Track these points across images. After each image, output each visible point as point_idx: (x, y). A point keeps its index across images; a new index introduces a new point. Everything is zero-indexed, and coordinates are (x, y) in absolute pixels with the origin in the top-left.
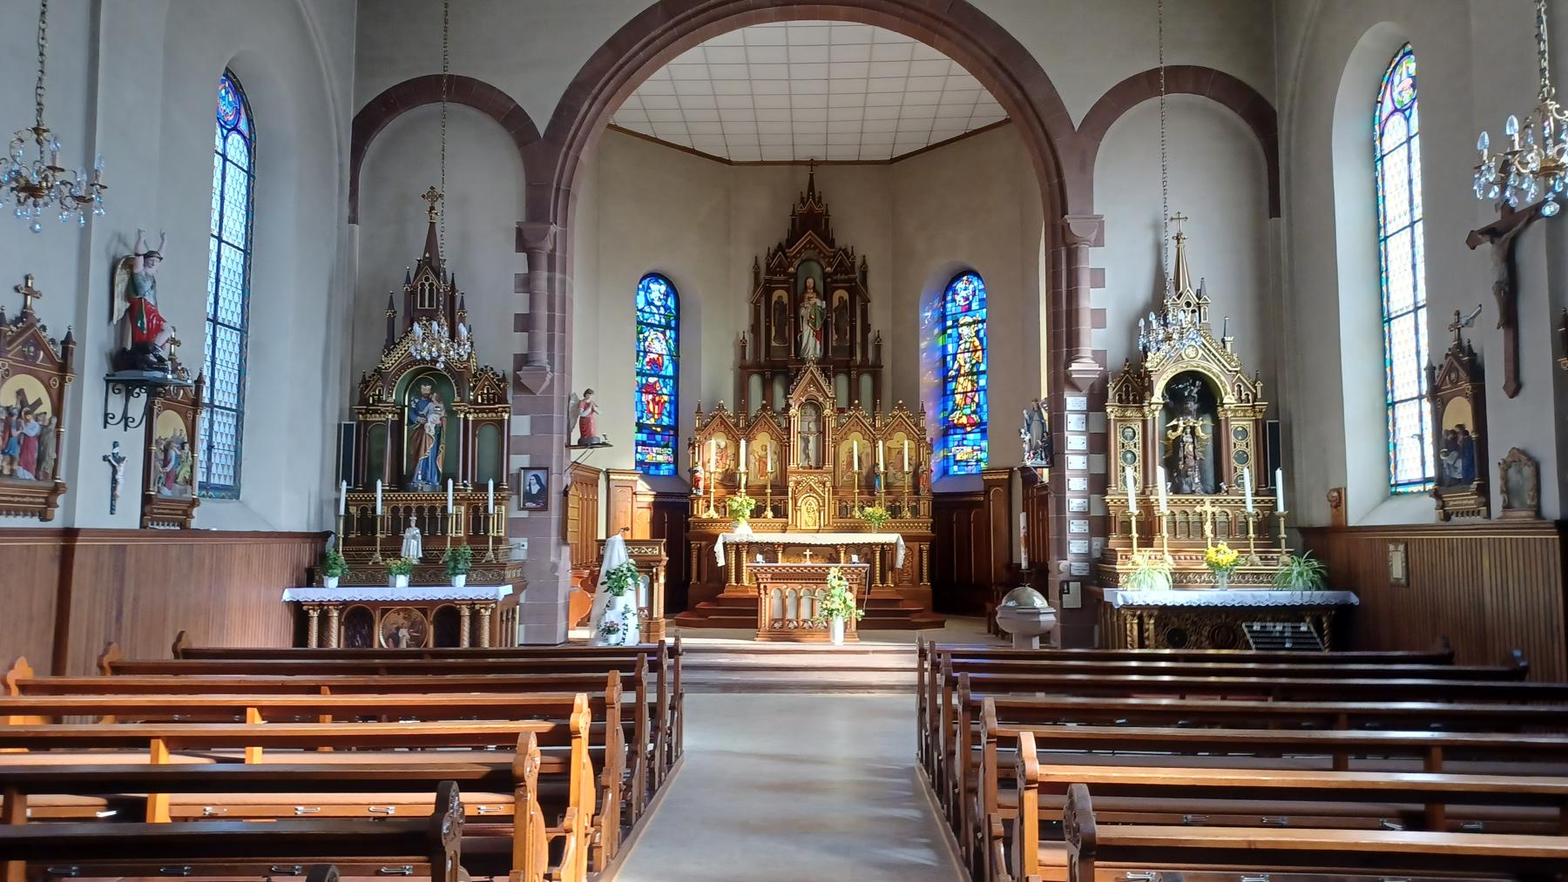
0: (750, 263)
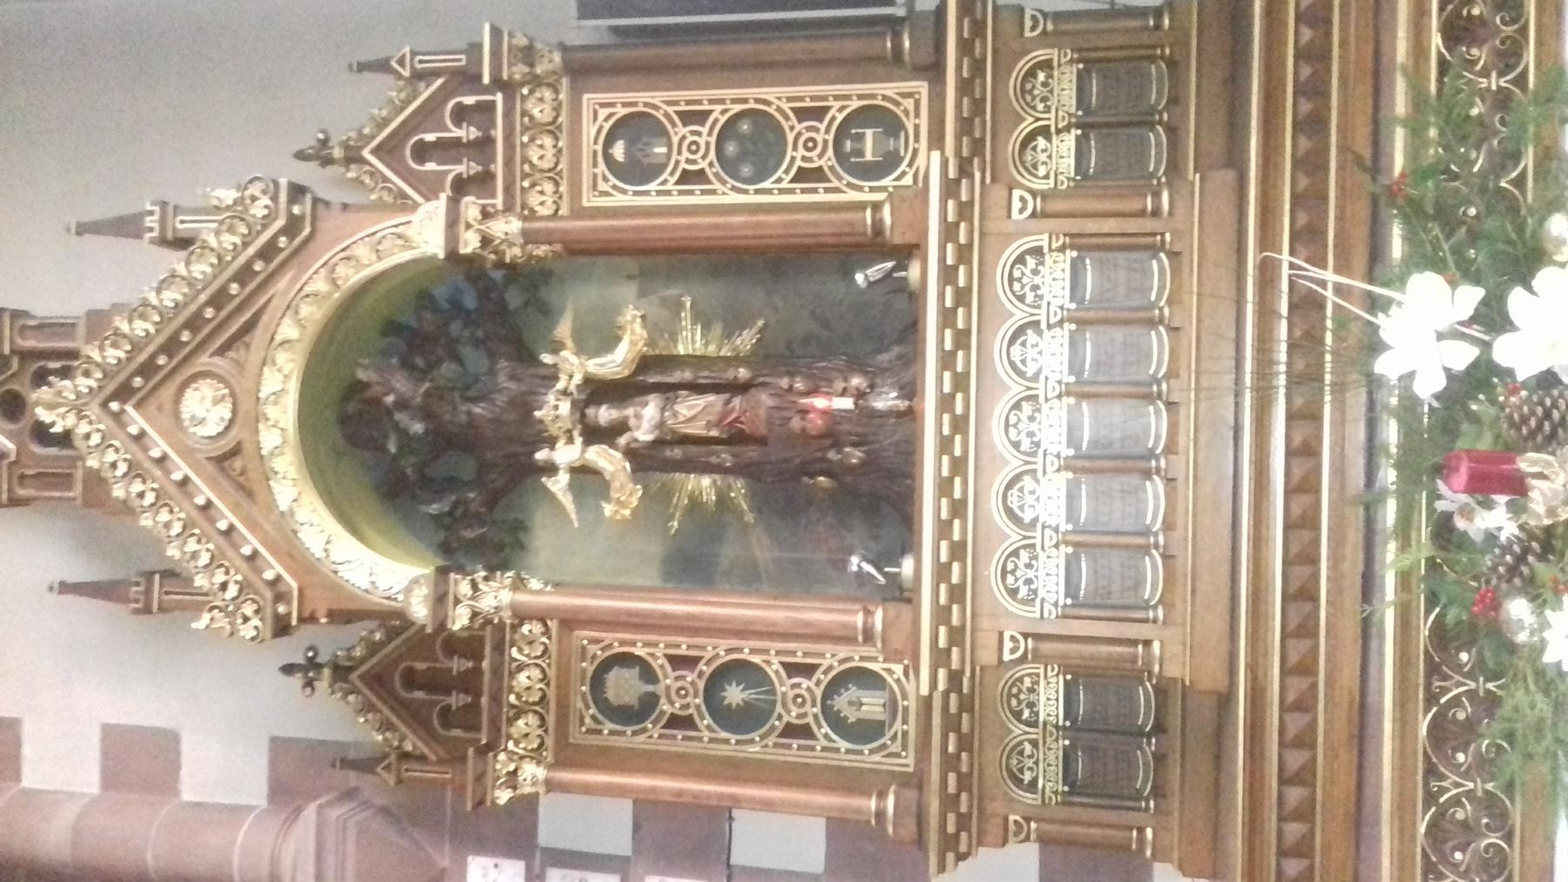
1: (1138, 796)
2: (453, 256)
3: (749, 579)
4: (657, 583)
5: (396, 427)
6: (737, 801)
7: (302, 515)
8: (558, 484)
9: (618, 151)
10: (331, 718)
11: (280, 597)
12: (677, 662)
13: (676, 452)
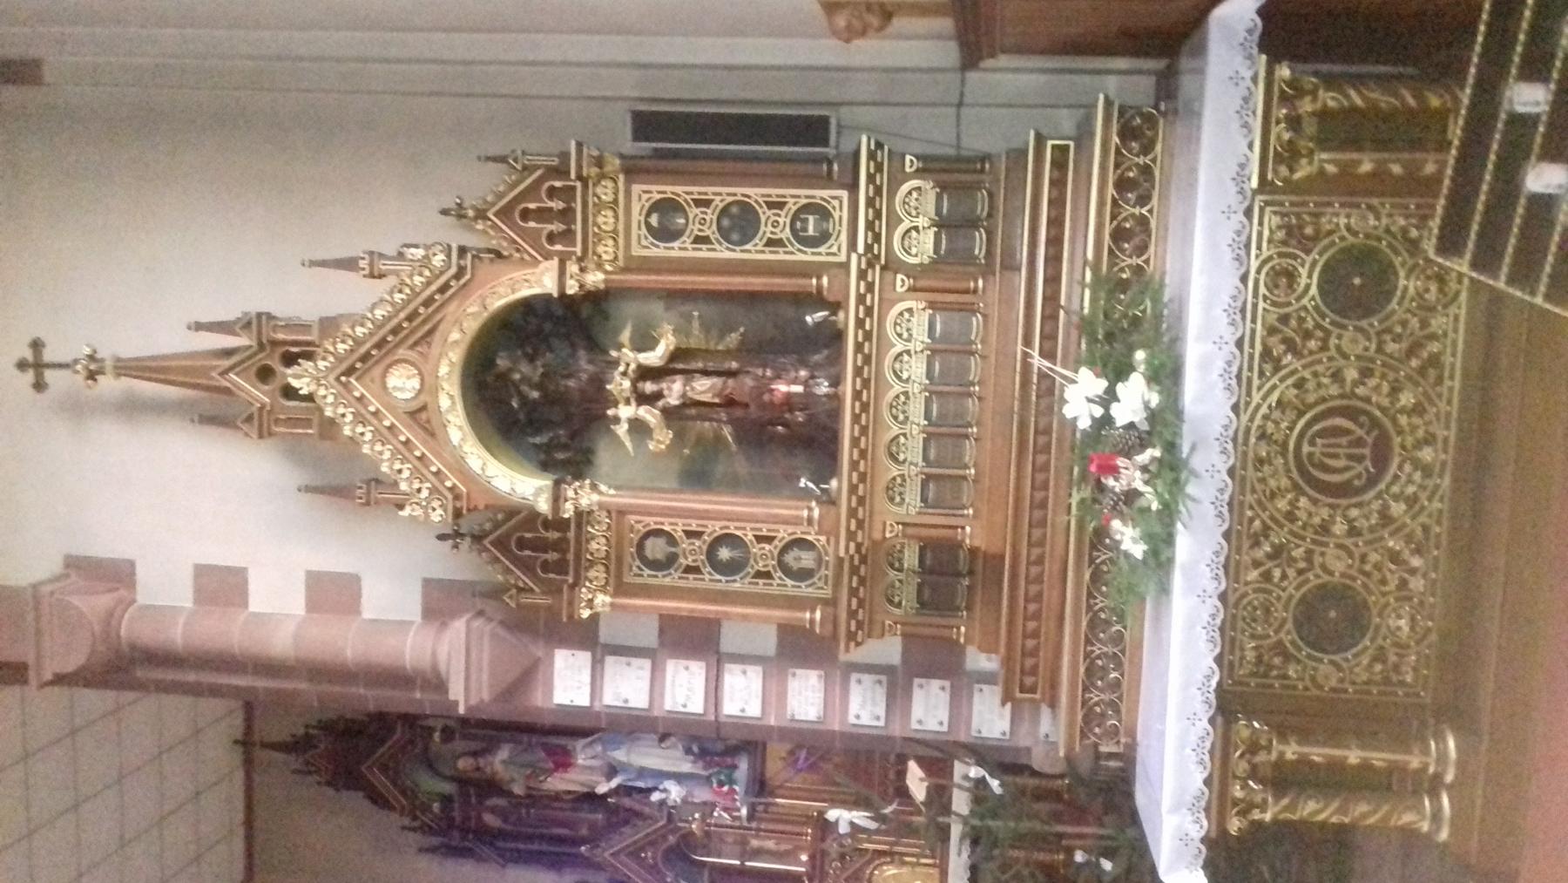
0: (424, 862)
1: (958, 609)
2: (563, 295)
3: (734, 485)
4: (675, 485)
5: (520, 393)
6: (727, 616)
7: (467, 448)
8: (622, 430)
9: (654, 220)
10: (461, 565)
11: (457, 497)
12: (690, 534)
13: (693, 411)
